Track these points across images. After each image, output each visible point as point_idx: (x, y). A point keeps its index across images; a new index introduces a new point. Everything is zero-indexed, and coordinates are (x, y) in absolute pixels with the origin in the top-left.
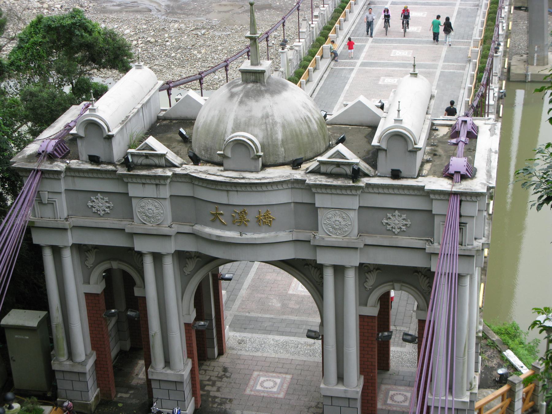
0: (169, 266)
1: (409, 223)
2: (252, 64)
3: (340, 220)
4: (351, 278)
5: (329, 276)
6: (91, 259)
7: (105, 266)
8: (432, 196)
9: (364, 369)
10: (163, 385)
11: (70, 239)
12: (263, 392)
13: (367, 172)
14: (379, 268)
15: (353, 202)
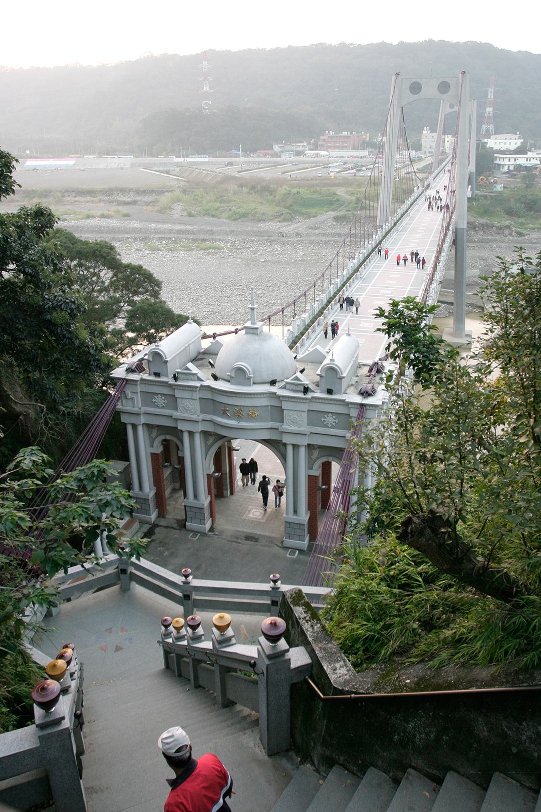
0: (198, 438)
1: (337, 421)
2: (251, 324)
3: (297, 417)
4: (303, 452)
5: (290, 450)
6: (155, 433)
7: (162, 437)
8: (350, 406)
9: (311, 507)
10: (193, 509)
11: (143, 419)
12: (253, 518)
13: (313, 389)
14: (321, 447)
15: (306, 407)
